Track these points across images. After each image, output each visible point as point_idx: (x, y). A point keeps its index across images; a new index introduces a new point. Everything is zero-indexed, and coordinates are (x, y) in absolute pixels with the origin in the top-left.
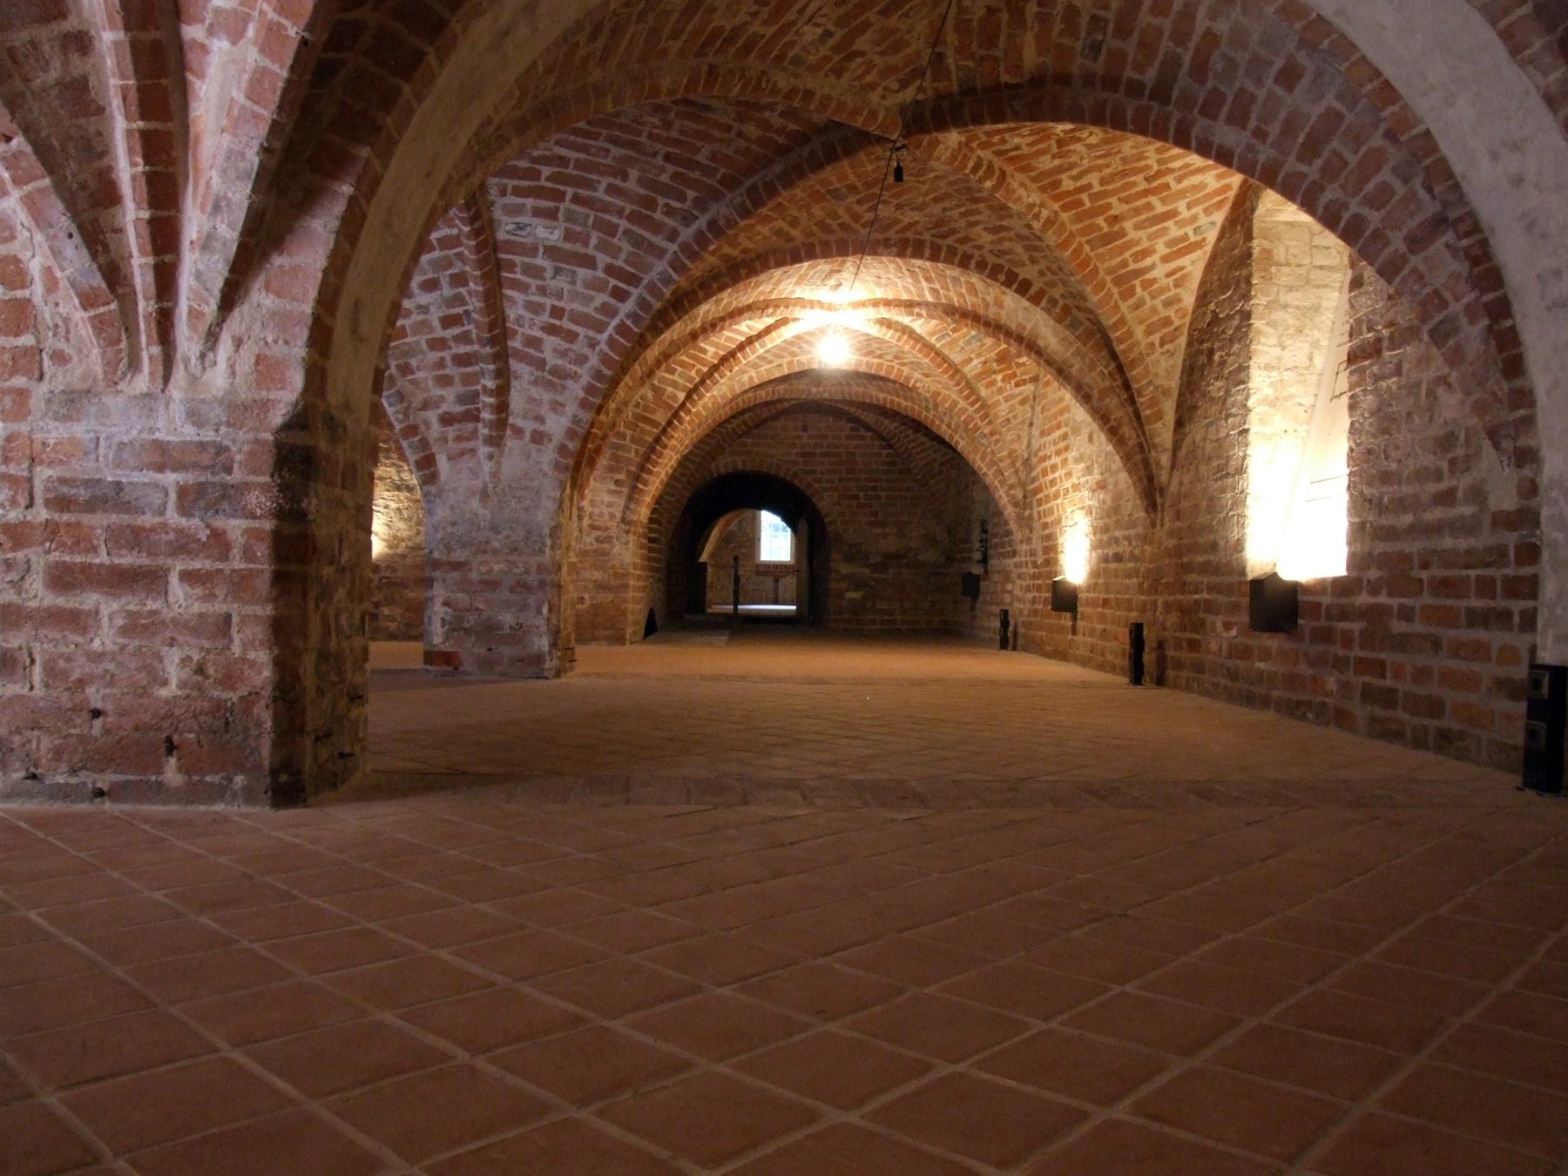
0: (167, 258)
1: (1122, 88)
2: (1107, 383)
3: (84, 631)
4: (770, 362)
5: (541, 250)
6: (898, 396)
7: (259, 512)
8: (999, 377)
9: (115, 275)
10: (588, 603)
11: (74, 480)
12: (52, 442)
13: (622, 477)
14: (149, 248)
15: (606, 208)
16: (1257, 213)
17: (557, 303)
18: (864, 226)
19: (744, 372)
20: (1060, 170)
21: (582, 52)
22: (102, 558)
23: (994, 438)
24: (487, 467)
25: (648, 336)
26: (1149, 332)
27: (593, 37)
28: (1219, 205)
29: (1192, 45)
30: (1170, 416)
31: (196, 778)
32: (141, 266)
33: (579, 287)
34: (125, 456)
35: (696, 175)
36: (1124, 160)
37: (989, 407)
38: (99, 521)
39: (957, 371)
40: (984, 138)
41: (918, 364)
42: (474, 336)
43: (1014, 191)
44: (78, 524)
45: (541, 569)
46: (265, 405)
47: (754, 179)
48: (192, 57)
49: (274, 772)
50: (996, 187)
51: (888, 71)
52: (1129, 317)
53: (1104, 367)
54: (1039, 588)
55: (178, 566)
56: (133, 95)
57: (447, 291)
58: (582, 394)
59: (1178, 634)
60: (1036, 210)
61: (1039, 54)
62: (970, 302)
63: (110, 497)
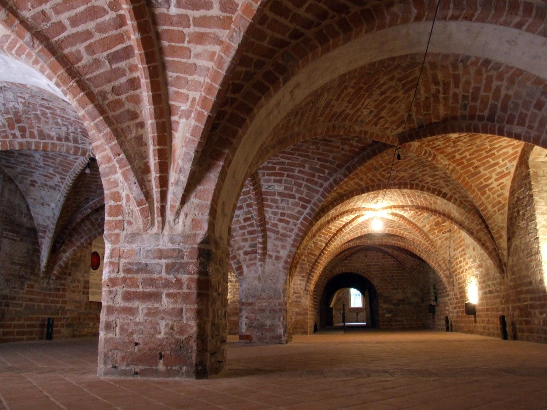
0: (164, 189)
1: (476, 119)
2: (479, 227)
3: (133, 315)
4: (354, 232)
5: (277, 194)
6: (399, 241)
7: (193, 272)
8: (436, 231)
9: (148, 195)
10: (294, 320)
11: (132, 263)
12: (126, 251)
13: (304, 274)
14: (159, 185)
15: (298, 178)
16: (530, 159)
17: (282, 211)
18: (386, 179)
19: (345, 236)
20: (455, 152)
21: (292, 121)
22: (140, 289)
23: (437, 253)
24: (260, 269)
25: (314, 222)
26: (493, 206)
27: (296, 117)
28: (514, 159)
29: (500, 100)
30: (505, 237)
31: (169, 368)
32: (156, 192)
33: (290, 205)
34: (149, 254)
35: (328, 164)
36: (477, 146)
37: (433, 242)
38: (140, 277)
39: (421, 230)
40: (427, 143)
41: (406, 229)
42: (255, 224)
43: (439, 160)
44: (133, 278)
45: (280, 304)
46: (195, 235)
47: (348, 164)
48: (174, 126)
49: (197, 366)
50: (433, 160)
51: (392, 123)
52: (485, 202)
53: (477, 221)
54: (459, 307)
55: (165, 291)
56: (156, 139)
57: (245, 209)
58: (292, 242)
59: (520, 319)
60: (447, 167)
61: (445, 111)
62: (425, 203)
63: (143, 268)
